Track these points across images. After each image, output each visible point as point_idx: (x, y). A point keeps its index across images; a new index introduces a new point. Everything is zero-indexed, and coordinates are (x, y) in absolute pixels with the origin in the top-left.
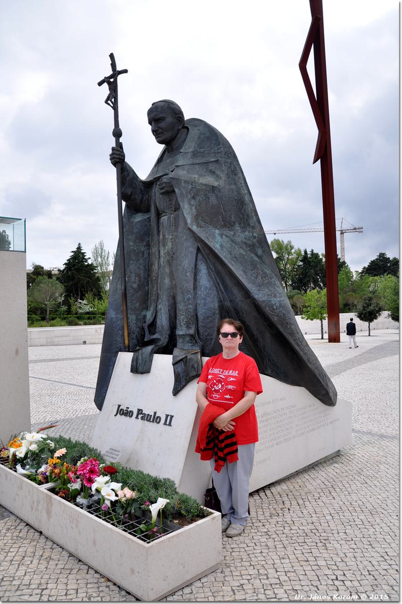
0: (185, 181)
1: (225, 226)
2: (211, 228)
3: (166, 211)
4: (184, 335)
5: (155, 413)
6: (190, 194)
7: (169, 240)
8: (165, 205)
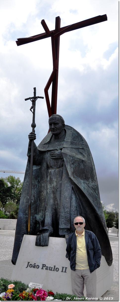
0: (69, 155)
1: (85, 179)
2: (79, 179)
3: (53, 167)
4: (63, 228)
5: (55, 266)
6: (71, 162)
7: (55, 182)
8: (53, 164)
